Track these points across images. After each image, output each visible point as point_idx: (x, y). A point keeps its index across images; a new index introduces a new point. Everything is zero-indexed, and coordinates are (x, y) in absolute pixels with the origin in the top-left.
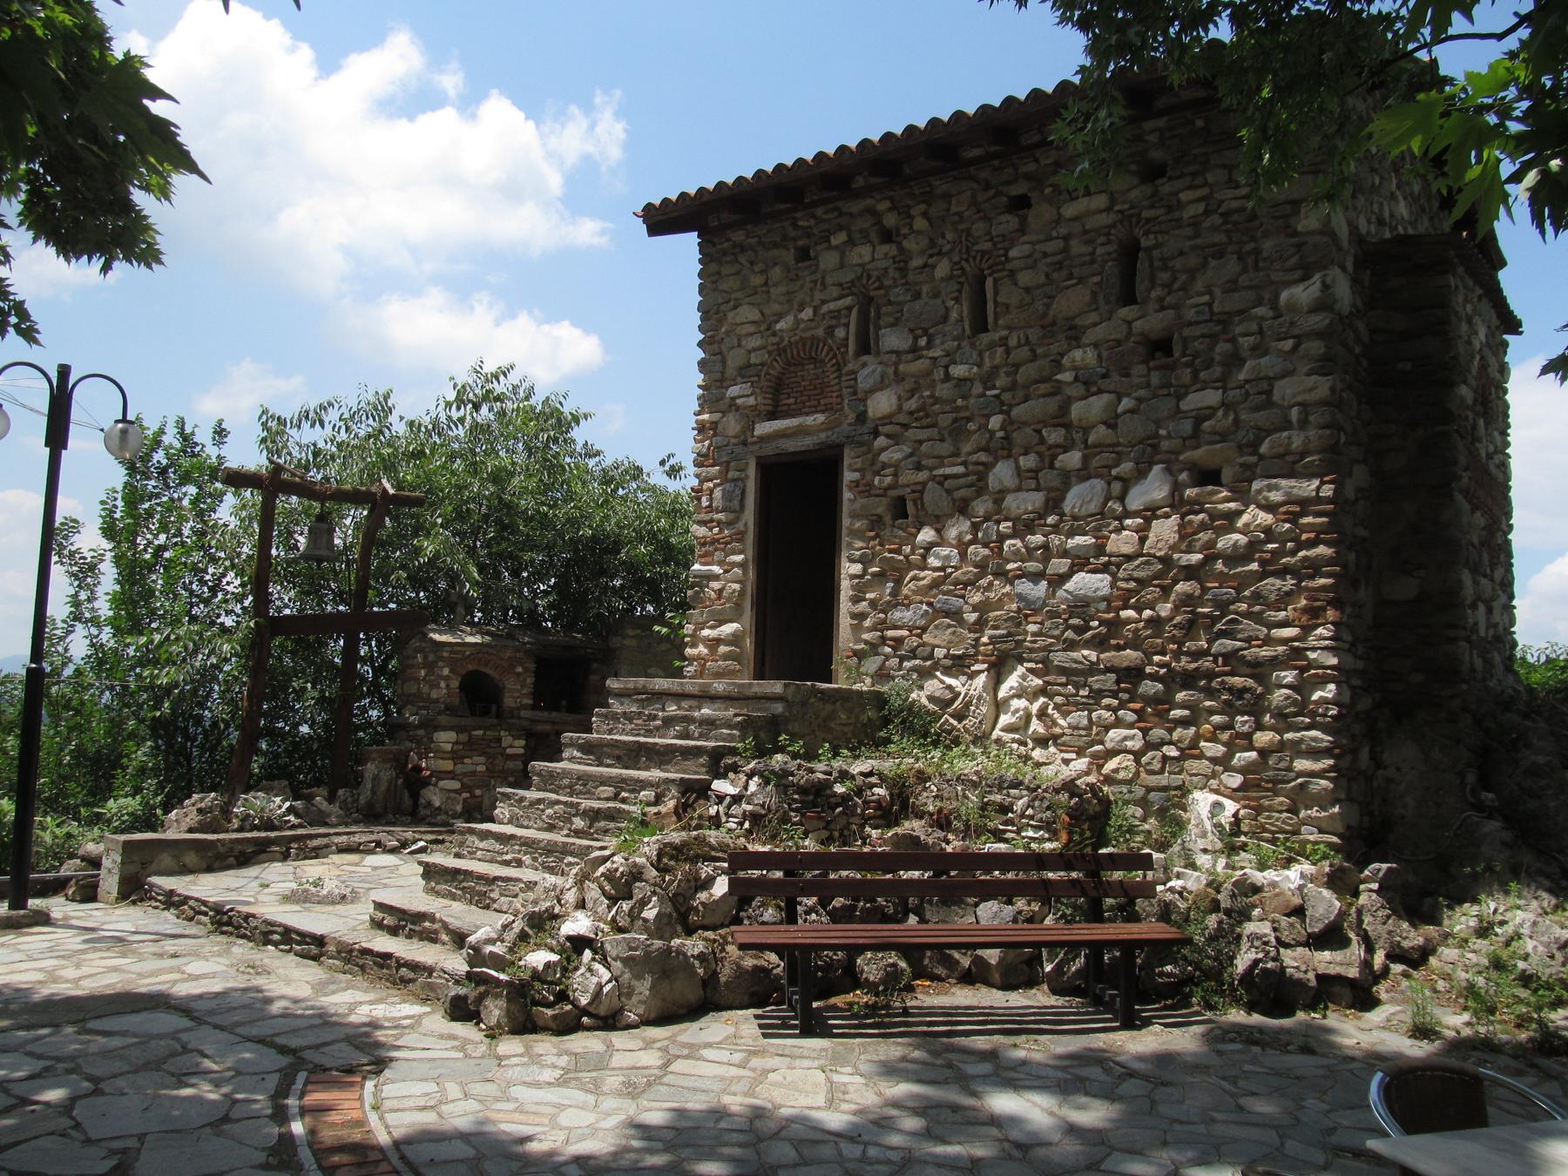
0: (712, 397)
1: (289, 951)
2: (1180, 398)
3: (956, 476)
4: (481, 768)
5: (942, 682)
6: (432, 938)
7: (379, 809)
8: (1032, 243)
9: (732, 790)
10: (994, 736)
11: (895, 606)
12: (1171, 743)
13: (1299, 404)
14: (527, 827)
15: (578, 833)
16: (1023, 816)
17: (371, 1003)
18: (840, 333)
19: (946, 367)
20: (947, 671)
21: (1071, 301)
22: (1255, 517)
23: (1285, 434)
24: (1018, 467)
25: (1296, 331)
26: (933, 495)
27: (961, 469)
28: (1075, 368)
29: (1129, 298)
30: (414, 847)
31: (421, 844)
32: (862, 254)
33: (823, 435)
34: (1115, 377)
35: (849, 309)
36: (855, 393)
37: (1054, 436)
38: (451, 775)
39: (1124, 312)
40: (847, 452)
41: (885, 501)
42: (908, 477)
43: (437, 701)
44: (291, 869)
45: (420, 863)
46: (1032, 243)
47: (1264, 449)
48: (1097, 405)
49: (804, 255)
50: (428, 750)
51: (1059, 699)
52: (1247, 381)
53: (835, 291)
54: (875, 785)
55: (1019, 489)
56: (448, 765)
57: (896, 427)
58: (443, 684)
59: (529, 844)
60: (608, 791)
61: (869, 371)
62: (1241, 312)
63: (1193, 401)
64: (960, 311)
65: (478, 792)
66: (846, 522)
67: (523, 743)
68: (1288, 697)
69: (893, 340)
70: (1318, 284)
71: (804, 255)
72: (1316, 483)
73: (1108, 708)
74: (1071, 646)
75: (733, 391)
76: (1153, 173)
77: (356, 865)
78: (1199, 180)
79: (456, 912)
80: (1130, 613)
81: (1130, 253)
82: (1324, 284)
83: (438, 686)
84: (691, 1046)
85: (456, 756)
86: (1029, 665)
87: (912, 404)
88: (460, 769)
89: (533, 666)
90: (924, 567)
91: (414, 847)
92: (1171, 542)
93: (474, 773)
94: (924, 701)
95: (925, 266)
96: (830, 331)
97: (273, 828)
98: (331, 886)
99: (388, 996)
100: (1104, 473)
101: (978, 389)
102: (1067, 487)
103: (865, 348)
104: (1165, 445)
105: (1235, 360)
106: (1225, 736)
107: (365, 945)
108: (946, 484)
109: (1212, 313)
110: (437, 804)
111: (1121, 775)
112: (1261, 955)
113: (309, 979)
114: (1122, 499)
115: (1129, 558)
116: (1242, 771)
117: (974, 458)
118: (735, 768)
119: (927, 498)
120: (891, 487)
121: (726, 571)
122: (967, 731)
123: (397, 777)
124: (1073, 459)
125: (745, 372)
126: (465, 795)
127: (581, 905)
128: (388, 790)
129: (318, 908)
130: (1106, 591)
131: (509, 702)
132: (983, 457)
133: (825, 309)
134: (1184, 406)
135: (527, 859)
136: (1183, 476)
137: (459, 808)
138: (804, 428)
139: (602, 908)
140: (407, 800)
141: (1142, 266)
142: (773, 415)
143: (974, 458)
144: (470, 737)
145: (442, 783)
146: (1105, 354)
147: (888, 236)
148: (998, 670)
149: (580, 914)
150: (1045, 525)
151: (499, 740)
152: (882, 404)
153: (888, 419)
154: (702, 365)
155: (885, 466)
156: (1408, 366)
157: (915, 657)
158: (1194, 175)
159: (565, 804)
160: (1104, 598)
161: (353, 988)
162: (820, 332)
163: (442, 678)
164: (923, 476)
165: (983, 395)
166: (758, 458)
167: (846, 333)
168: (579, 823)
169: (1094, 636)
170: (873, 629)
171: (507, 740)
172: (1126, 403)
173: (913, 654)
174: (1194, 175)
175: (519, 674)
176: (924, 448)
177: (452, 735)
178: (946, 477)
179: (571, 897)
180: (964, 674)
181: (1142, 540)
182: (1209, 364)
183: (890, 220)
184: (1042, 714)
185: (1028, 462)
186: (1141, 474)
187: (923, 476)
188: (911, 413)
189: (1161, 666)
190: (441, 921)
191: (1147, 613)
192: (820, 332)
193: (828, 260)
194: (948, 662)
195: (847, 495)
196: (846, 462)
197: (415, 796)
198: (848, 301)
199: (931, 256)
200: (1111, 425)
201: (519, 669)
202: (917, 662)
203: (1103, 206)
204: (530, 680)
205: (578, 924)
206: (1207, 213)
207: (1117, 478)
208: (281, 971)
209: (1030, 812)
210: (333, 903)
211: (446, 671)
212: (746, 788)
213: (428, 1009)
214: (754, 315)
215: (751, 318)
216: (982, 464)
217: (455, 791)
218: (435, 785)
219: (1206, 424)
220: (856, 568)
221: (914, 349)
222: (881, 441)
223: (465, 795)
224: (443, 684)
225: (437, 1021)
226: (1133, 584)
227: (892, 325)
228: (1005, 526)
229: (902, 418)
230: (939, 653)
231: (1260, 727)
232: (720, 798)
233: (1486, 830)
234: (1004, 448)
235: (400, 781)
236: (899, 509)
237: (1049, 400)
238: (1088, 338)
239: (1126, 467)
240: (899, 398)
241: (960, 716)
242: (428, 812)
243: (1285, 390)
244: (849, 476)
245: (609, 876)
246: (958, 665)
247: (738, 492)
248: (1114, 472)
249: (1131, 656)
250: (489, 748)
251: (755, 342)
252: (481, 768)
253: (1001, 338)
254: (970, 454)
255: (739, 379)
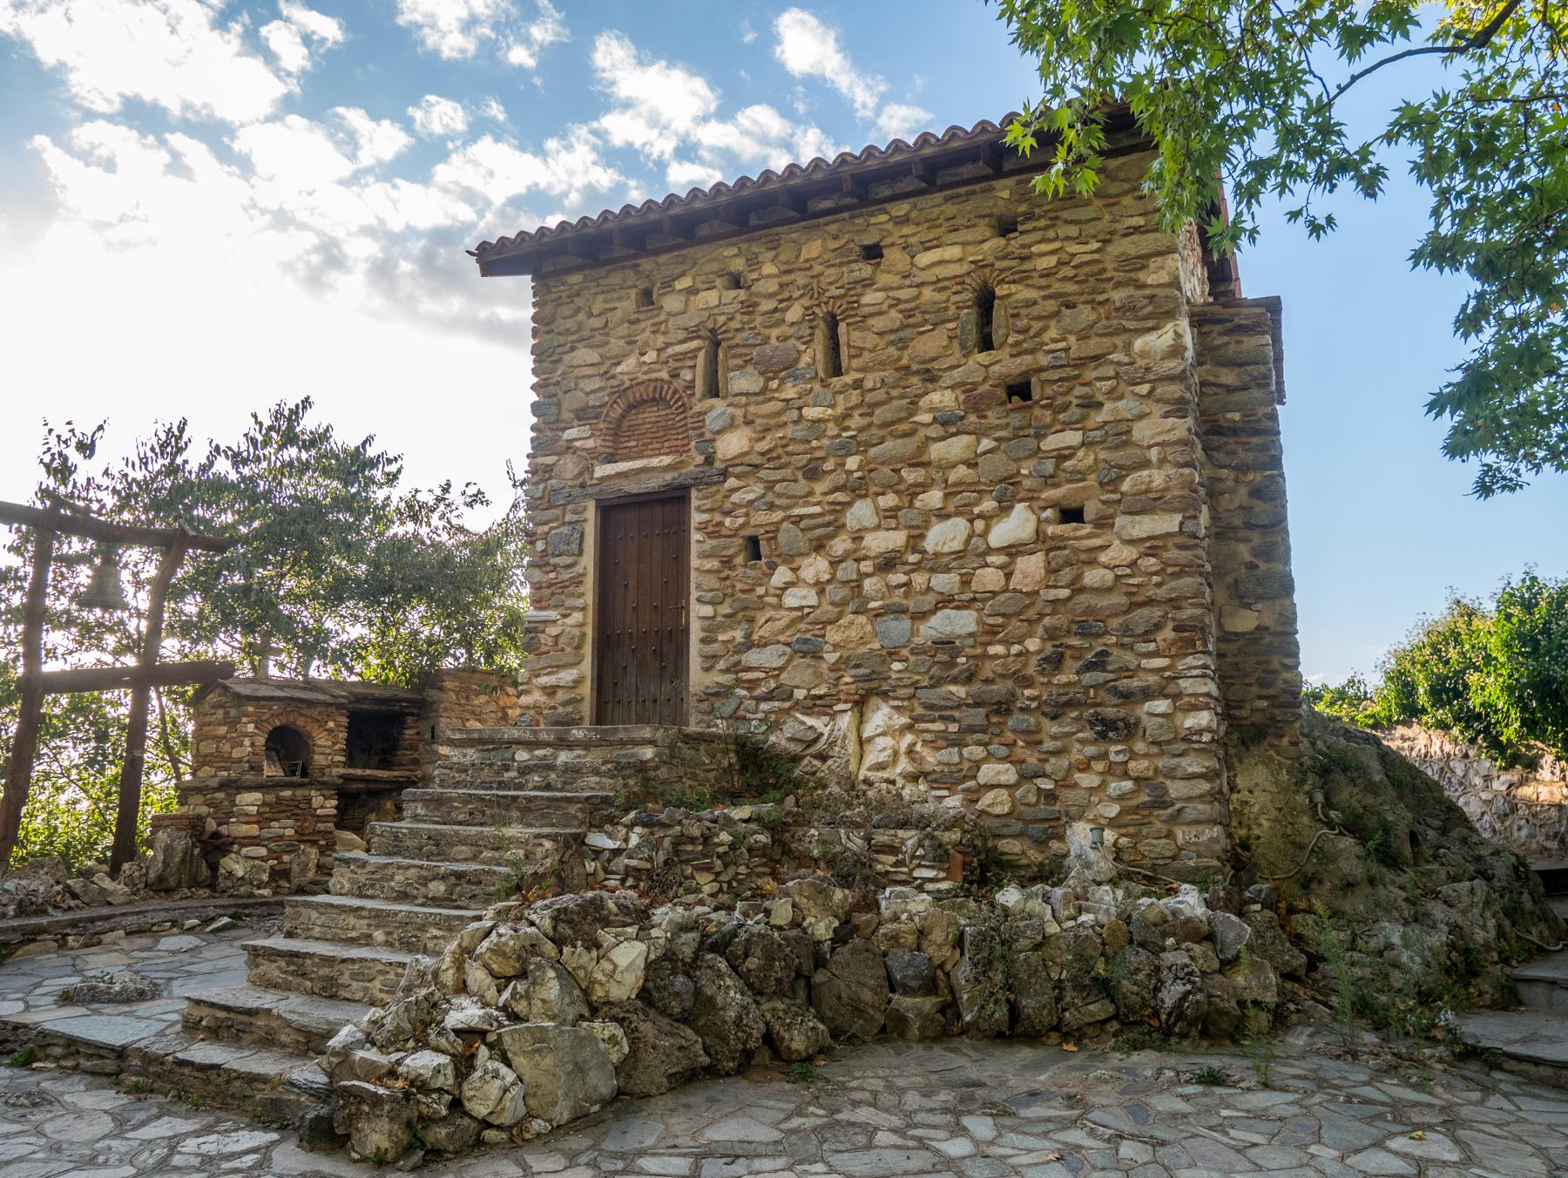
0: (545, 440)
1: (76, 1068)
2: (1040, 436)
3: (812, 516)
4: (290, 832)
5: (803, 723)
6: (267, 1042)
7: (172, 883)
8: (964, 244)
9: (609, 844)
10: (861, 777)
11: (750, 648)
12: (1045, 775)
13: (1158, 444)
14: (372, 897)
15: (435, 901)
16: (913, 857)
17: (197, 1134)
18: (687, 375)
19: (800, 409)
20: (808, 711)
21: (929, 344)
22: (1120, 553)
23: (1145, 473)
24: (877, 507)
25: (1151, 376)
26: (788, 534)
27: (817, 509)
28: (931, 410)
29: (986, 344)
30: (214, 926)
31: (226, 920)
32: (711, 297)
33: (669, 477)
34: (972, 418)
35: (700, 349)
36: (702, 435)
37: (911, 476)
38: (255, 841)
39: (983, 358)
40: (694, 493)
41: (738, 541)
42: (761, 517)
43: (240, 761)
44: (69, 961)
45: (244, 948)
46: (964, 244)
47: (1125, 486)
48: (957, 447)
49: (647, 297)
50: (230, 814)
51: (928, 737)
52: (1106, 423)
53: (682, 335)
54: (755, 832)
55: (878, 528)
56: (253, 830)
57: (749, 467)
58: (247, 742)
59: (378, 917)
60: (465, 850)
61: (718, 410)
62: (1096, 358)
63: (1052, 442)
64: (813, 355)
65: (286, 858)
66: (695, 562)
67: (334, 802)
68: (1162, 726)
69: (743, 382)
70: (1171, 334)
71: (647, 297)
72: (1178, 518)
73: (978, 743)
74: (937, 682)
75: (569, 434)
76: (1006, 227)
77: (150, 949)
78: (1051, 234)
79: (296, 1008)
80: (998, 649)
81: (985, 302)
82: (1176, 332)
83: (241, 745)
84: (622, 1156)
85: (262, 820)
86: (896, 703)
87: (763, 446)
88: (266, 833)
89: (344, 721)
90: (779, 606)
91: (214, 926)
92: (1038, 578)
93: (281, 837)
94: (783, 742)
95: (775, 310)
96: (675, 375)
97: (41, 911)
98: (123, 978)
99: (218, 1122)
100: (963, 511)
101: (832, 430)
102: (927, 525)
103: (713, 391)
104: (1027, 483)
105: (1091, 404)
106: (1099, 766)
107: (180, 1055)
108: (802, 525)
109: (1068, 357)
110: (240, 873)
111: (998, 810)
112: (1189, 987)
113: (107, 1106)
114: (984, 534)
115: (994, 594)
116: (1120, 798)
117: (831, 498)
118: (612, 820)
119: (781, 538)
120: (742, 526)
121: (565, 616)
122: (831, 771)
123: (194, 846)
124: (934, 498)
125: (582, 415)
126: (272, 862)
127: (462, 988)
128: (183, 861)
129: (109, 1008)
130: (973, 628)
131: (320, 759)
132: (841, 497)
133: (670, 351)
134: (1045, 445)
135: (379, 935)
136: (1049, 513)
137: (265, 877)
138: (651, 468)
139: (491, 994)
140: (205, 871)
141: (999, 314)
142: (611, 459)
143: (831, 498)
144: (277, 797)
145: (244, 850)
146: (962, 397)
147: (736, 282)
148: (860, 705)
149: (463, 1001)
150: (906, 563)
151: (309, 801)
152: (732, 444)
153: (733, 462)
154: (535, 408)
155: (736, 506)
156: (1237, 416)
157: (771, 699)
158: (1046, 228)
159: (421, 867)
160: (971, 635)
161: (169, 1113)
162: (664, 375)
163: (246, 735)
164: (777, 516)
165: (839, 436)
166: (598, 501)
167: (696, 375)
168: (438, 888)
169: (961, 673)
170: (727, 671)
171: (317, 800)
172: (986, 444)
173: (769, 697)
174: (1046, 228)
175: (331, 731)
176: (778, 488)
177: (256, 796)
178: (802, 517)
179: (448, 977)
180: (826, 714)
181: (1008, 576)
182: (1065, 408)
183: (738, 265)
184: (910, 751)
185: (889, 500)
186: (1004, 509)
187: (777, 516)
188: (763, 454)
189: (1032, 699)
190: (279, 1017)
191: (1015, 649)
192: (664, 375)
193: (672, 303)
194: (809, 703)
195: (696, 536)
196: (694, 503)
197: (214, 867)
198: (695, 344)
199: (781, 301)
200: (971, 464)
201: (331, 724)
202: (776, 704)
203: (958, 256)
204: (343, 735)
205: (466, 1012)
206: (1060, 263)
207: (980, 516)
208: (67, 1098)
209: (920, 852)
210: (128, 1001)
211: (251, 728)
212: (626, 840)
213: (275, 1136)
214: (594, 357)
215: (590, 361)
216: (839, 503)
217: (262, 859)
218: (238, 853)
219: (1067, 463)
220: (708, 610)
221: (764, 390)
222: (732, 482)
223: (272, 862)
224: (247, 742)
225: (290, 1158)
226: (1000, 620)
227: (740, 368)
228: (866, 566)
229: (756, 460)
230: (800, 694)
231: (1133, 756)
232: (597, 853)
233: (1341, 846)
234: (857, 489)
235: (196, 851)
236: (753, 547)
237: (906, 440)
238: (947, 379)
239: (988, 505)
240: (750, 440)
241: (823, 757)
242: (229, 884)
243: (1143, 432)
244: (696, 518)
245: (497, 951)
246: (817, 705)
247: (577, 535)
248: (976, 510)
249: (1001, 687)
250: (297, 811)
251: (596, 383)
252: (290, 832)
253: (855, 381)
254: (825, 494)
255: (575, 423)
